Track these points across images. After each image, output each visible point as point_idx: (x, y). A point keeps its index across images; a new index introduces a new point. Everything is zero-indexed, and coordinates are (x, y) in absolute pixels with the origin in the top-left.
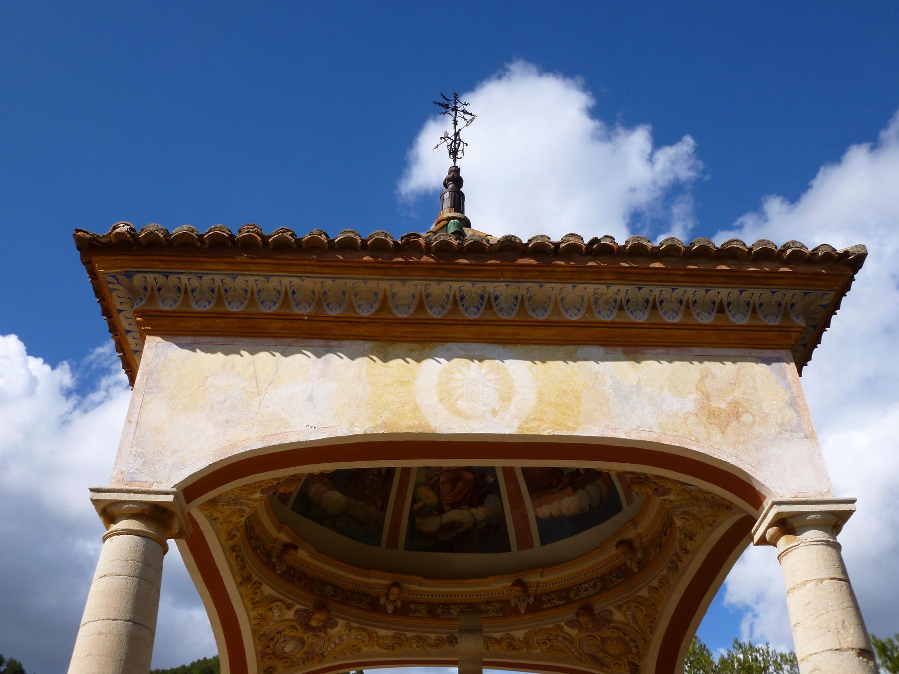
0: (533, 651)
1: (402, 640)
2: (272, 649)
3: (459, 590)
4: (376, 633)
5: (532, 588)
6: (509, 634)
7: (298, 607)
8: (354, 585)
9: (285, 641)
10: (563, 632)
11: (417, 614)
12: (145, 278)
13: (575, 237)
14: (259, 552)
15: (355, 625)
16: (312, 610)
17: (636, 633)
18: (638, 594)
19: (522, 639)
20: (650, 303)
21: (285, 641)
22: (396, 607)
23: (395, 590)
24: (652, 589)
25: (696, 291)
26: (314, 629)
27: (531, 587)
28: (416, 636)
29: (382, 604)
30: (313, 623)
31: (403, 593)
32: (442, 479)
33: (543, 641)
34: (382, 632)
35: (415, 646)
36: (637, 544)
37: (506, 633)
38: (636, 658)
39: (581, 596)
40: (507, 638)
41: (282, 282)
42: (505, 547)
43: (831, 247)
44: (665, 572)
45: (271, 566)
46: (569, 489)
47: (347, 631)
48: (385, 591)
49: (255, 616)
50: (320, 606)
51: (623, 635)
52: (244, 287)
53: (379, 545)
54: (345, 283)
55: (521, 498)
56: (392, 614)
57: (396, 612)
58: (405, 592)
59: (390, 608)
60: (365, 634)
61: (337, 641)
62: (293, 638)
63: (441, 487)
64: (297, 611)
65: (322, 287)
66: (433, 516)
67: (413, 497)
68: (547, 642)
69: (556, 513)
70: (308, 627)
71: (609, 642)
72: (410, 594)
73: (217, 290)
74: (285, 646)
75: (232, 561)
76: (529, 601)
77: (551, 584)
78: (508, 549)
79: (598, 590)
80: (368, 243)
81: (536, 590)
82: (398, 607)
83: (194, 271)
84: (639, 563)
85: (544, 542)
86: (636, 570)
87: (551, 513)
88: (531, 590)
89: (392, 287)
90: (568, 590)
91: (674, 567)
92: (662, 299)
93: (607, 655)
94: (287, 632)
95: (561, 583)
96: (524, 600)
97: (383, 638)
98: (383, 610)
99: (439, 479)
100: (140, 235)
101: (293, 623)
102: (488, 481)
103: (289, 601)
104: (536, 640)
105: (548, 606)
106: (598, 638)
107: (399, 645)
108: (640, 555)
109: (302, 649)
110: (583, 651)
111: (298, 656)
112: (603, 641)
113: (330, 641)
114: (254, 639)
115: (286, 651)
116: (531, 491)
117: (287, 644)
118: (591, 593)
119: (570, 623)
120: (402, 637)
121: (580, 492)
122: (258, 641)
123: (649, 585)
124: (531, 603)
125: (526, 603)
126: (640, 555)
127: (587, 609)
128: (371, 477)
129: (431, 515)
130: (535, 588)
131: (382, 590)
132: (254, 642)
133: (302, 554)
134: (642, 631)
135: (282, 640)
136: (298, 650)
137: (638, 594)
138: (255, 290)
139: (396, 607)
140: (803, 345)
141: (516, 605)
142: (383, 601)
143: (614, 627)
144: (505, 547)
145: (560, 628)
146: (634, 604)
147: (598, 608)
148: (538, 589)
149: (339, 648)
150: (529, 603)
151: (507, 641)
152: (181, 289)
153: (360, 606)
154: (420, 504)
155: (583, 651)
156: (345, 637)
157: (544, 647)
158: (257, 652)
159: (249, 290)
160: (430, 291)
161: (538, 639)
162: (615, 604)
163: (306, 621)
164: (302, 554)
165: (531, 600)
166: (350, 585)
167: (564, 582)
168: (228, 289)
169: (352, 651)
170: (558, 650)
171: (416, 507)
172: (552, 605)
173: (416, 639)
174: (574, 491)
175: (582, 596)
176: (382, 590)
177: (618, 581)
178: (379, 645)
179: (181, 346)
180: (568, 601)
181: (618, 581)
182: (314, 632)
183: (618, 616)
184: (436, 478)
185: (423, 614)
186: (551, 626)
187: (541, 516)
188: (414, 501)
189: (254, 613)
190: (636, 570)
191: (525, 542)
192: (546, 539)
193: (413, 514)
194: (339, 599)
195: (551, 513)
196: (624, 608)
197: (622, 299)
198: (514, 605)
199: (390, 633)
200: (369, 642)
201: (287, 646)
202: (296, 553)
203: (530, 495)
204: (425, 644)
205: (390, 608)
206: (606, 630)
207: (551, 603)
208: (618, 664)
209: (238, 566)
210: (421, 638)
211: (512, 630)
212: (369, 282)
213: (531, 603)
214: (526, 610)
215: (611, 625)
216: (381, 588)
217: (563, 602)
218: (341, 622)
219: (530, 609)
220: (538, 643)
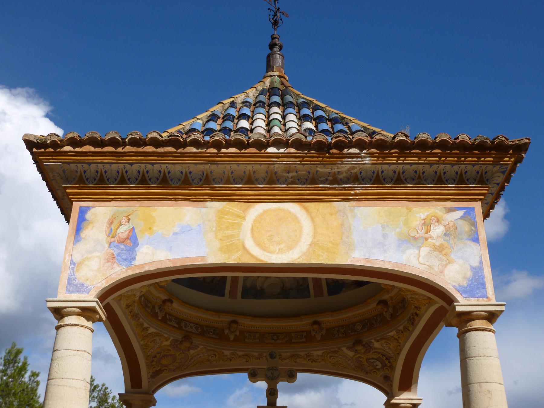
3: (264, 324)
13: (382, 135)
20: (141, 173)
22: (236, 335)
23: (234, 325)
25: (466, 167)
31: (238, 326)
41: (78, 166)
42: (221, 294)
44: (256, 354)
65: (167, 169)
73: (121, 171)
78: (223, 295)
80: (290, 142)
86: (389, 319)
89: (231, 167)
92: (383, 171)
100: (146, 139)
108: (391, 310)
133: (175, 305)
138: (103, 171)
139: (236, 335)
142: (226, 332)
144: (221, 294)
150: (322, 334)
152: (161, 172)
159: (99, 171)
160: (191, 170)
164: (175, 305)
179: (97, 309)
180: (180, 328)
181: (214, 336)
186: (166, 336)
190: (389, 319)
191: (233, 295)
192: (330, 294)
197: (378, 170)
202: (172, 305)
208: (388, 369)
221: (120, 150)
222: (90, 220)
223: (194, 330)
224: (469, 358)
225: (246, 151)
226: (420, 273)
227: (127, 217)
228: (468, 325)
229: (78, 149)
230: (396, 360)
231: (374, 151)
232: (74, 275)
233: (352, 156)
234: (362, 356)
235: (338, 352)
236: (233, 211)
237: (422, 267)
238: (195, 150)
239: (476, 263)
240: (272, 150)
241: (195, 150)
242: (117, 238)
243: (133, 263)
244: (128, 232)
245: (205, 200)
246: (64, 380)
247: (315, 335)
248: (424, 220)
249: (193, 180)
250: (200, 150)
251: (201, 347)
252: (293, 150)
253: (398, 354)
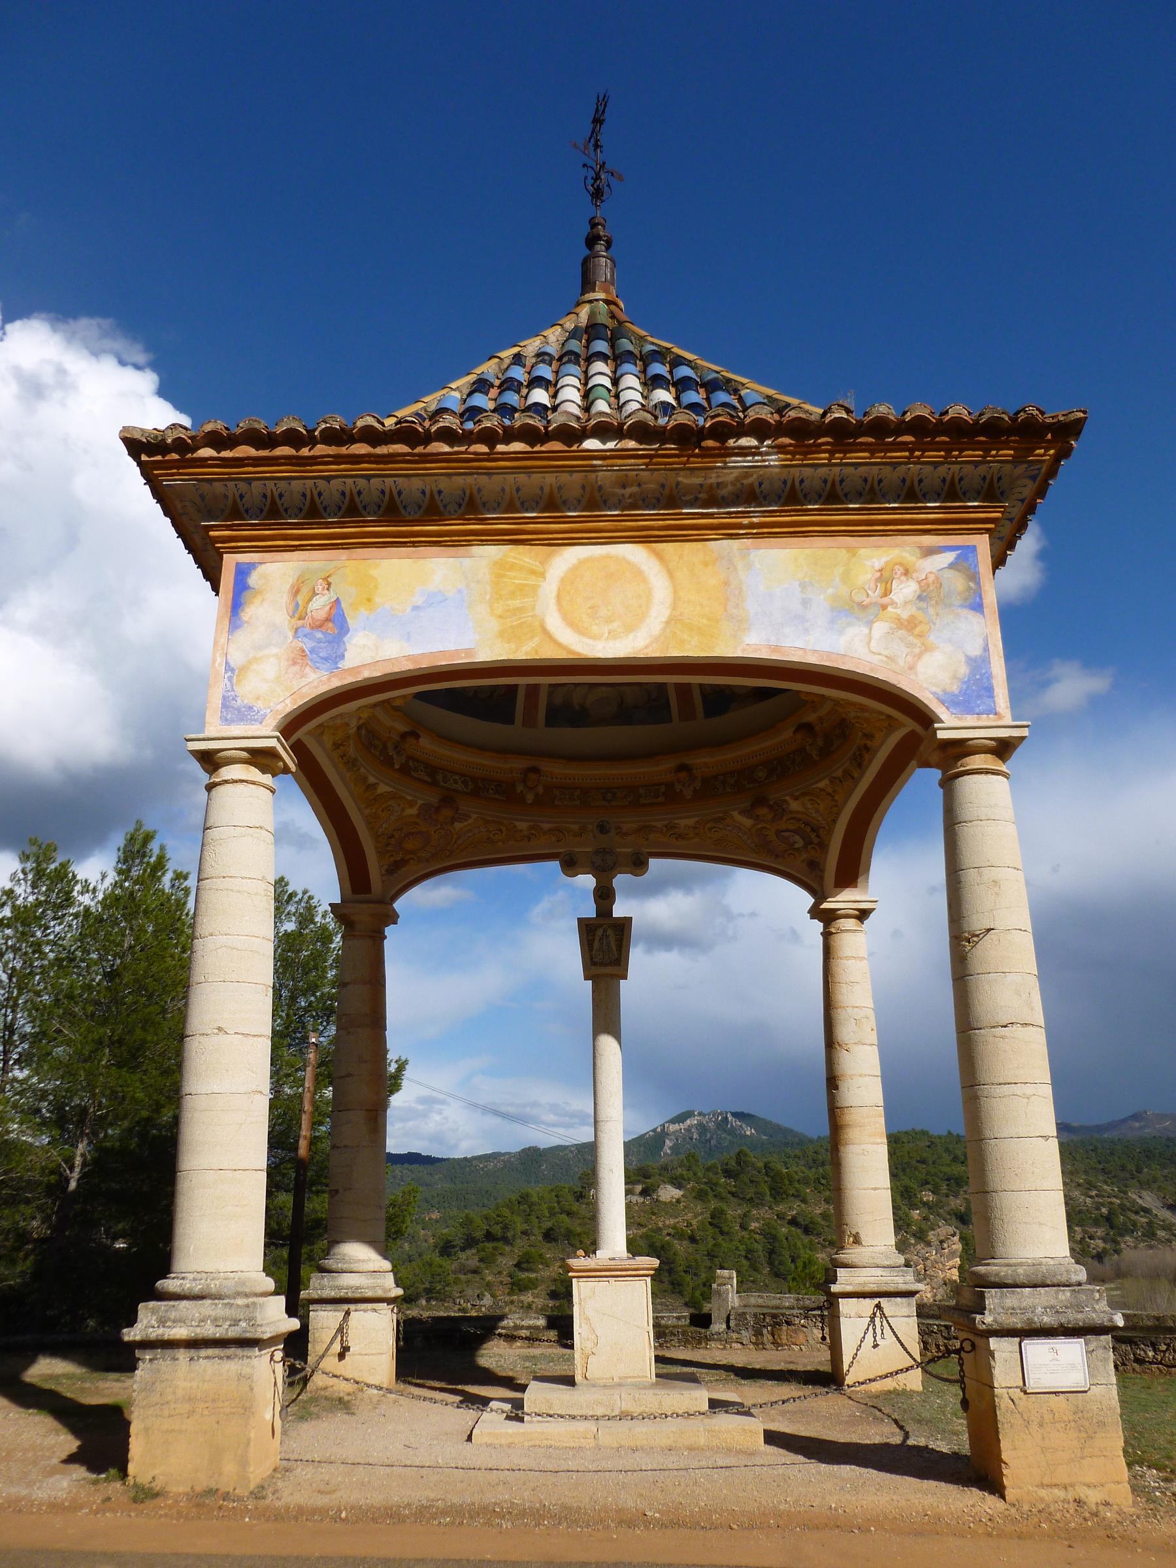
12: (226, 485)
23: (533, 776)
29: (519, 791)
43: (265, 1252)
45: (388, 761)
52: (341, 488)
54: (315, 483)
59: (530, 798)
82: (541, 793)
83: (745, 464)
133: (425, 742)
140: (999, 538)
142: (520, 788)
143: (792, 818)
164: (425, 742)
168: (283, 492)
181: (497, 796)
183: (794, 805)
204: (566, 834)
205: (530, 798)
212: (534, 476)
221: (305, 452)
222: (256, 587)
224: (960, 823)
225: (543, 449)
226: (872, 670)
227: (325, 579)
228: (959, 763)
229: (226, 454)
230: (830, 832)
231: (786, 440)
232: (233, 690)
233: (744, 452)
235: (724, 819)
236: (521, 563)
237: (876, 660)
238: (446, 448)
239: (975, 650)
240: (591, 444)
241: (446, 448)
242: (308, 620)
243: (340, 666)
244: (328, 607)
245: (469, 544)
246: (227, 879)
247: (681, 790)
248: (880, 571)
249: (445, 506)
250: (456, 449)
251: (474, 816)
252: (632, 444)
253: (834, 821)
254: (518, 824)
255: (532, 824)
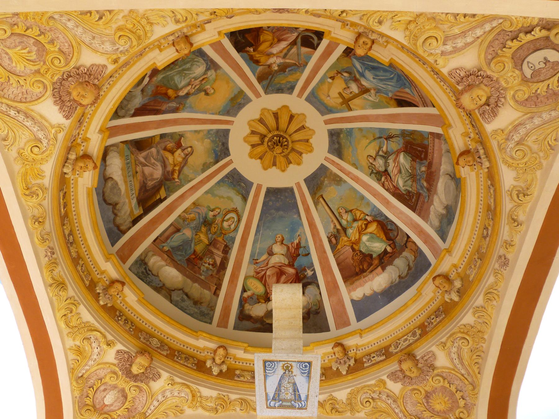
0: (357, 415)
1: (226, 401)
2: (91, 400)
4: (199, 392)
5: (352, 351)
6: (331, 395)
7: (119, 347)
8: (182, 346)
9: (105, 390)
10: (386, 388)
11: (242, 379)
14: (79, 268)
15: (178, 380)
16: (134, 355)
17: (462, 378)
18: (462, 323)
19: (344, 401)
21: (105, 390)
24: (477, 310)
26: (135, 378)
27: (351, 351)
28: (241, 399)
30: (135, 370)
32: (268, 273)
33: (367, 400)
34: (206, 392)
35: (238, 409)
36: (453, 276)
37: (329, 394)
38: (465, 412)
39: (400, 347)
40: (329, 400)
46: (379, 268)
47: (170, 385)
48: (212, 355)
49: (72, 347)
50: (142, 352)
51: (448, 386)
53: (211, 323)
55: (336, 286)
56: (217, 376)
57: (221, 374)
58: (231, 358)
59: (215, 371)
60: (188, 390)
61: (160, 398)
62: (115, 387)
63: (267, 279)
64: (118, 352)
66: (260, 304)
67: (243, 286)
68: (371, 400)
69: (368, 292)
70: (128, 373)
71: (434, 395)
72: (236, 362)
74: (105, 397)
75: (36, 240)
76: (350, 363)
77: (370, 345)
78: (328, 330)
79: (418, 336)
81: (356, 354)
82: (224, 371)
84: (458, 291)
85: (359, 319)
87: (364, 294)
88: (351, 354)
90: (387, 348)
91: (505, 262)
93: (433, 415)
94: (107, 379)
95: (379, 343)
96: (345, 363)
97: (207, 398)
98: (209, 372)
99: (265, 273)
101: (114, 367)
102: (308, 274)
103: (110, 337)
104: (359, 399)
105: (368, 364)
106: (423, 392)
107: (222, 406)
109: (124, 404)
110: (407, 412)
111: (119, 412)
112: (428, 396)
113: (153, 398)
114: (70, 379)
115: (106, 403)
116: (346, 279)
117: (107, 394)
118: (411, 341)
119: (393, 376)
120: (226, 398)
121: (389, 268)
122: (74, 383)
123: (473, 306)
124: (352, 365)
125: (347, 365)
126: (458, 284)
127: (411, 356)
128: (207, 265)
129: (258, 303)
130: (355, 351)
131: (209, 354)
132: (71, 383)
134: (469, 374)
135: (102, 388)
136: (119, 404)
137: (462, 323)
141: (338, 368)
142: (209, 364)
145: (384, 382)
146: (460, 335)
147: (419, 353)
148: (358, 352)
149: (162, 408)
150: (349, 365)
151: (330, 402)
153: (186, 364)
154: (249, 293)
155: (407, 412)
156: (168, 394)
157: (368, 409)
158: (74, 398)
161: (362, 398)
162: (437, 344)
163: (128, 366)
165: (352, 362)
166: (178, 345)
167: (382, 341)
169: (174, 411)
170: (382, 412)
171: (245, 295)
172: (373, 362)
173: (240, 401)
174: (383, 269)
175: (402, 348)
176: (209, 354)
177: (438, 320)
178: (203, 408)
181: (438, 320)
182: (135, 381)
184: (263, 273)
185: (248, 379)
186: (373, 382)
187: (355, 298)
188: (244, 290)
189: (70, 343)
191: (342, 322)
193: (243, 302)
194: (165, 353)
195: (364, 294)
196: (449, 344)
198: (335, 369)
199: (214, 393)
200: (191, 403)
201: (107, 396)
203: (345, 282)
205: (215, 371)
206: (430, 380)
207: (372, 361)
209: (46, 256)
210: (245, 400)
211: (334, 391)
213: (352, 365)
214: (347, 371)
215: (436, 372)
216: (208, 352)
217: (384, 357)
218: (165, 375)
219: (351, 371)
220: (362, 404)
223: (411, 339)
234: (512, 93)
254: (464, 321)
255: (471, 311)
